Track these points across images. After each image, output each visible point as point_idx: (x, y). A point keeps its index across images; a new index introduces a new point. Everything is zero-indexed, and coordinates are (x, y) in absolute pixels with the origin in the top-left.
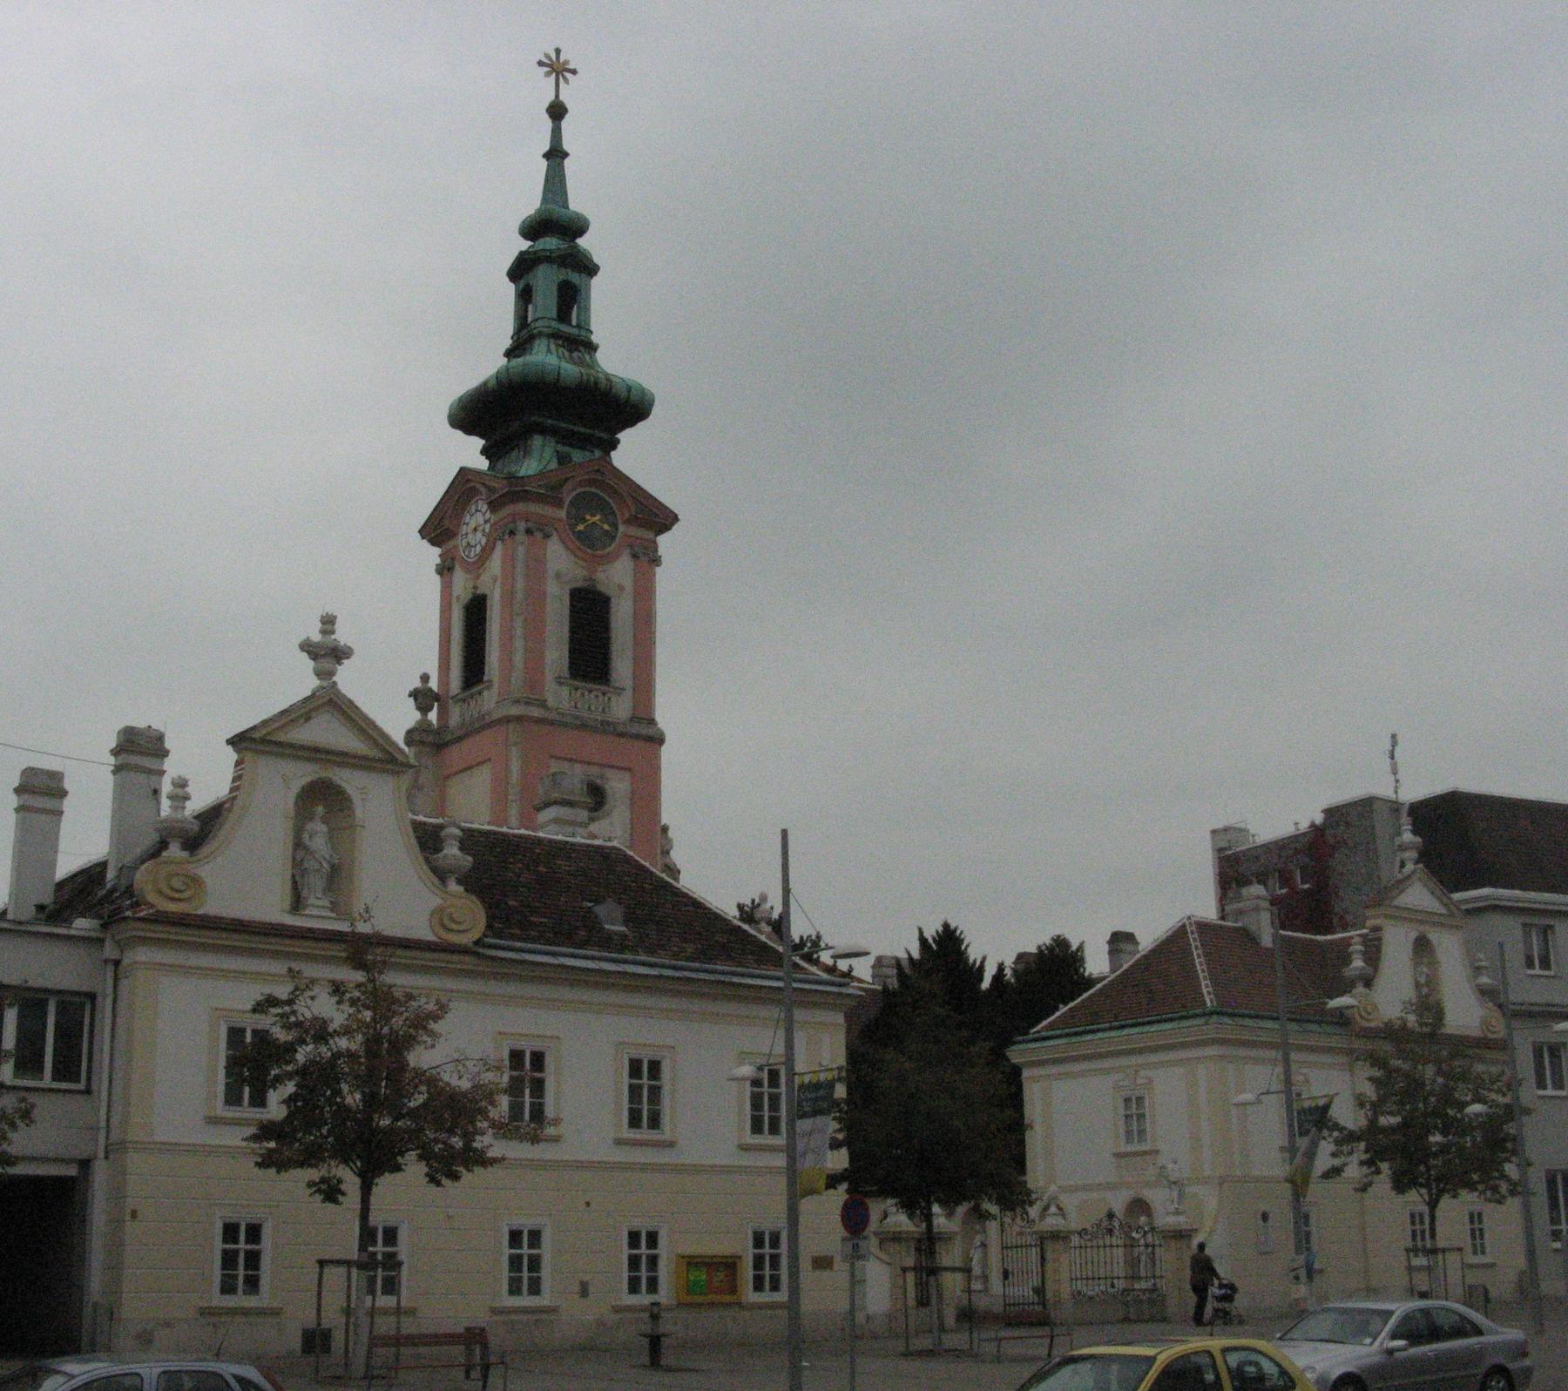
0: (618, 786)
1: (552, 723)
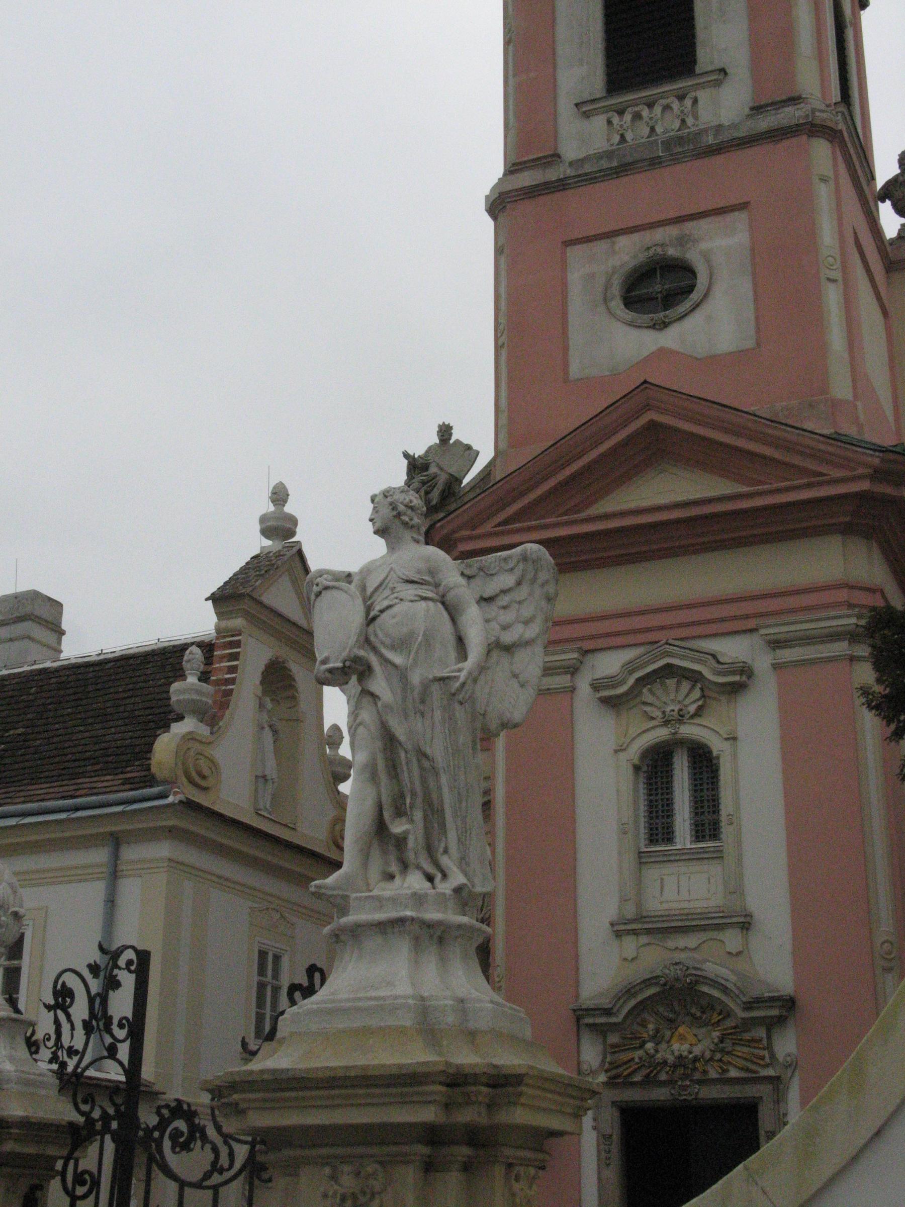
0: (721, 249)
1: (561, 185)
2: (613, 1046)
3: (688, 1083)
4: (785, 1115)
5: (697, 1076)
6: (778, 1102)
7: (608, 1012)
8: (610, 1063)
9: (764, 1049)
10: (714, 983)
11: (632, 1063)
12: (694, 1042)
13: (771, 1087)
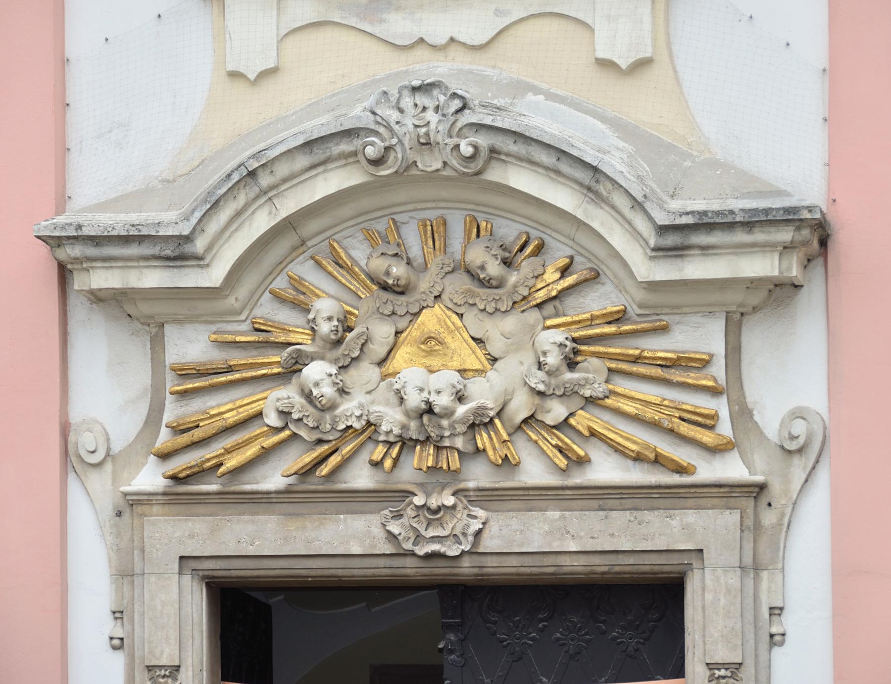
2: (184, 373)
3: (450, 501)
4: (776, 611)
5: (478, 476)
6: (753, 568)
7: (178, 252)
8: (178, 430)
9: (715, 392)
10: (561, 160)
11: (256, 430)
12: (472, 363)
13: (734, 517)
